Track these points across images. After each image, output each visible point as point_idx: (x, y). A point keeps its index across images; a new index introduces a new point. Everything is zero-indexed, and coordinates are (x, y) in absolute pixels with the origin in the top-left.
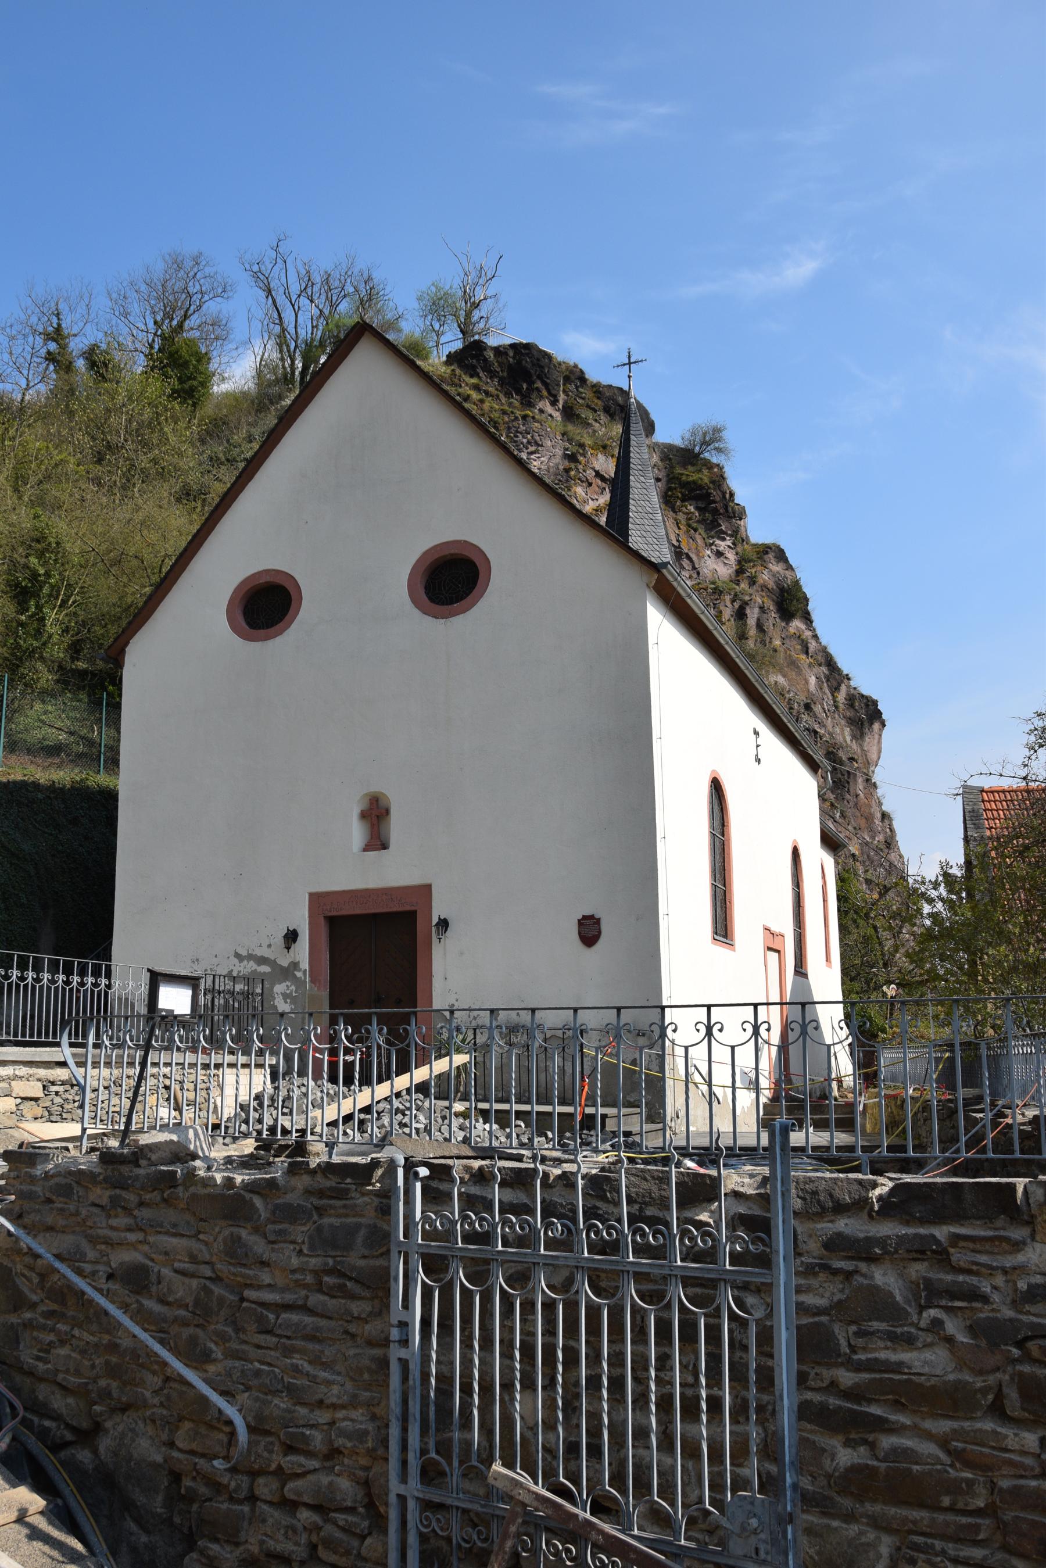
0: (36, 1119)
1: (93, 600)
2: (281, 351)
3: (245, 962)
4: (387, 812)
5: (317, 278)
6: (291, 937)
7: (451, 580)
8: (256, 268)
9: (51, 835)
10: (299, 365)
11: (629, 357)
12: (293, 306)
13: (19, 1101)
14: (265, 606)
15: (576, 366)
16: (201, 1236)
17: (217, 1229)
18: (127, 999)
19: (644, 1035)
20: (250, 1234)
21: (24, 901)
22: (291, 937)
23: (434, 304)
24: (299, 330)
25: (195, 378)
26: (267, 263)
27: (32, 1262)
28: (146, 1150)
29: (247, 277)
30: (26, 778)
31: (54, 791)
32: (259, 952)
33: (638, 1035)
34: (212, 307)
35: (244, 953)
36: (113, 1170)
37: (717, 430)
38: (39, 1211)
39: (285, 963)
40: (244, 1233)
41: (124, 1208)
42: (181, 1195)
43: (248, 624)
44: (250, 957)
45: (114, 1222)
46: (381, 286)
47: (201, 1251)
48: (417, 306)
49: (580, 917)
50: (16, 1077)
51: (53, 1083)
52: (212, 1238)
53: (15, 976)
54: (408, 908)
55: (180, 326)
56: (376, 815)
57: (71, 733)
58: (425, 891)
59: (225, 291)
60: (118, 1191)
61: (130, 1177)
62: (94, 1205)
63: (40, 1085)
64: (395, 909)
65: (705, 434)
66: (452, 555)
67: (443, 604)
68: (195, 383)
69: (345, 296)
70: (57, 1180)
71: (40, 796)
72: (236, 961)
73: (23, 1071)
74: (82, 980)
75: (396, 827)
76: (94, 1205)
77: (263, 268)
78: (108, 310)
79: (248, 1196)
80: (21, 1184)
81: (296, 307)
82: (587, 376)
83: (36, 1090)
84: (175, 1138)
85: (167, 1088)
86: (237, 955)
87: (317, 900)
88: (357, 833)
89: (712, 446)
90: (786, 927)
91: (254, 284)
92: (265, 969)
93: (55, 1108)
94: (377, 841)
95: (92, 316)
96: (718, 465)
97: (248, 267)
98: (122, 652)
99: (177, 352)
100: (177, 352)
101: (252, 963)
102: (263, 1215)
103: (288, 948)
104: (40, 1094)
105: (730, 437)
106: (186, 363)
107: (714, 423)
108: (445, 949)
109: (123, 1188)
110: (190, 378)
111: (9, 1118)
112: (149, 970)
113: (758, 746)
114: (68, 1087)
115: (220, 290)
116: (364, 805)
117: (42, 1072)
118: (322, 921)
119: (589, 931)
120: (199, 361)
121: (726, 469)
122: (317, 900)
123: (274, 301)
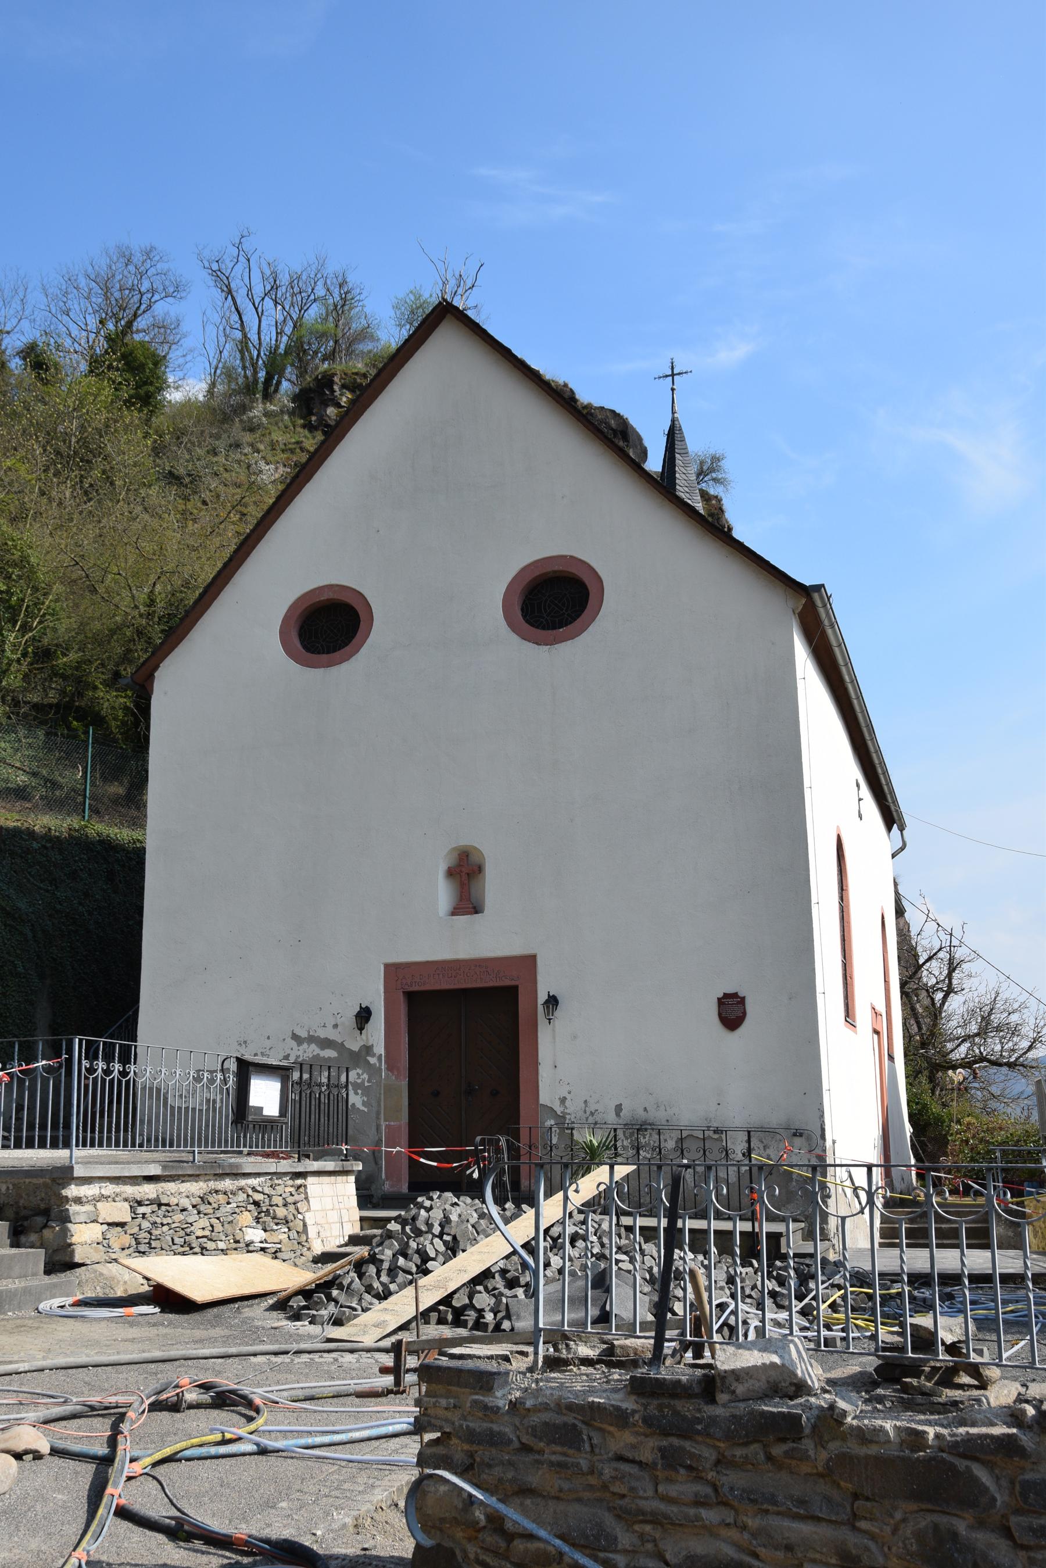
0: (123, 1249)
1: (51, 625)
2: (242, 359)
3: (305, 1045)
4: (480, 869)
5: (284, 280)
6: (364, 1016)
7: (554, 600)
8: (215, 267)
9: (47, 891)
10: (262, 375)
11: (672, 368)
12: (256, 309)
13: (105, 1227)
14: (328, 626)
15: (566, 385)
16: (863, 1525)
17: (898, 1515)
18: (159, 1090)
19: (801, 1135)
20: (971, 1527)
21: (20, 969)
22: (364, 1016)
23: (412, 312)
24: (262, 338)
25: (151, 383)
26: (227, 262)
27: (503, 1545)
28: (731, 1379)
29: (205, 274)
30: (19, 824)
31: (50, 841)
32: (322, 1034)
33: (795, 1135)
34: (161, 308)
35: (304, 1034)
36: (660, 1408)
37: (716, 459)
38: (511, 1463)
39: (355, 1047)
40: (961, 1527)
41: (690, 1468)
42: (811, 1453)
43: (305, 647)
44: (311, 1039)
45: (673, 1490)
46: (358, 291)
47: (867, 1549)
48: (393, 314)
49: (721, 995)
50: (103, 1198)
51: (140, 1203)
52: (888, 1529)
53: (100, 1070)
54: (507, 983)
55: (130, 324)
56: (466, 873)
57: (34, 774)
58: (530, 962)
59: (176, 291)
60: (675, 1441)
61: (699, 1421)
62: (620, 1458)
63: (126, 1205)
64: (491, 984)
65: (702, 463)
66: (555, 572)
67: (544, 628)
68: (151, 389)
69: (315, 300)
70: (546, 1417)
71: (35, 845)
72: (294, 1044)
73: (109, 1189)
74: (91, 1064)
75: (493, 887)
76: (620, 1458)
77: (223, 267)
78: (43, 307)
79: (961, 1464)
80: (464, 1418)
81: (260, 310)
82: (577, 397)
83: (121, 1212)
84: (776, 1359)
85: (256, 1204)
86: (295, 1037)
87: (394, 972)
88: (443, 894)
89: (709, 477)
90: (881, 1008)
91: (212, 283)
92: (330, 1053)
93: (143, 1235)
94: (468, 902)
95: (27, 313)
96: (716, 497)
97: (207, 265)
98: (150, 677)
99: (131, 354)
100: (131, 354)
101: (313, 1046)
102: (998, 1496)
103: (361, 1029)
104: (126, 1217)
105: (730, 467)
106: (142, 366)
107: (712, 451)
108: (554, 1030)
109: (684, 1436)
110: (145, 383)
111: (96, 1250)
112: (238, 1059)
113: (860, 800)
114: (155, 1207)
115: (171, 290)
116: (452, 861)
117: (129, 1190)
118: (401, 998)
119: (731, 1012)
120: (156, 364)
121: (724, 502)
122: (394, 972)
123: (235, 303)
